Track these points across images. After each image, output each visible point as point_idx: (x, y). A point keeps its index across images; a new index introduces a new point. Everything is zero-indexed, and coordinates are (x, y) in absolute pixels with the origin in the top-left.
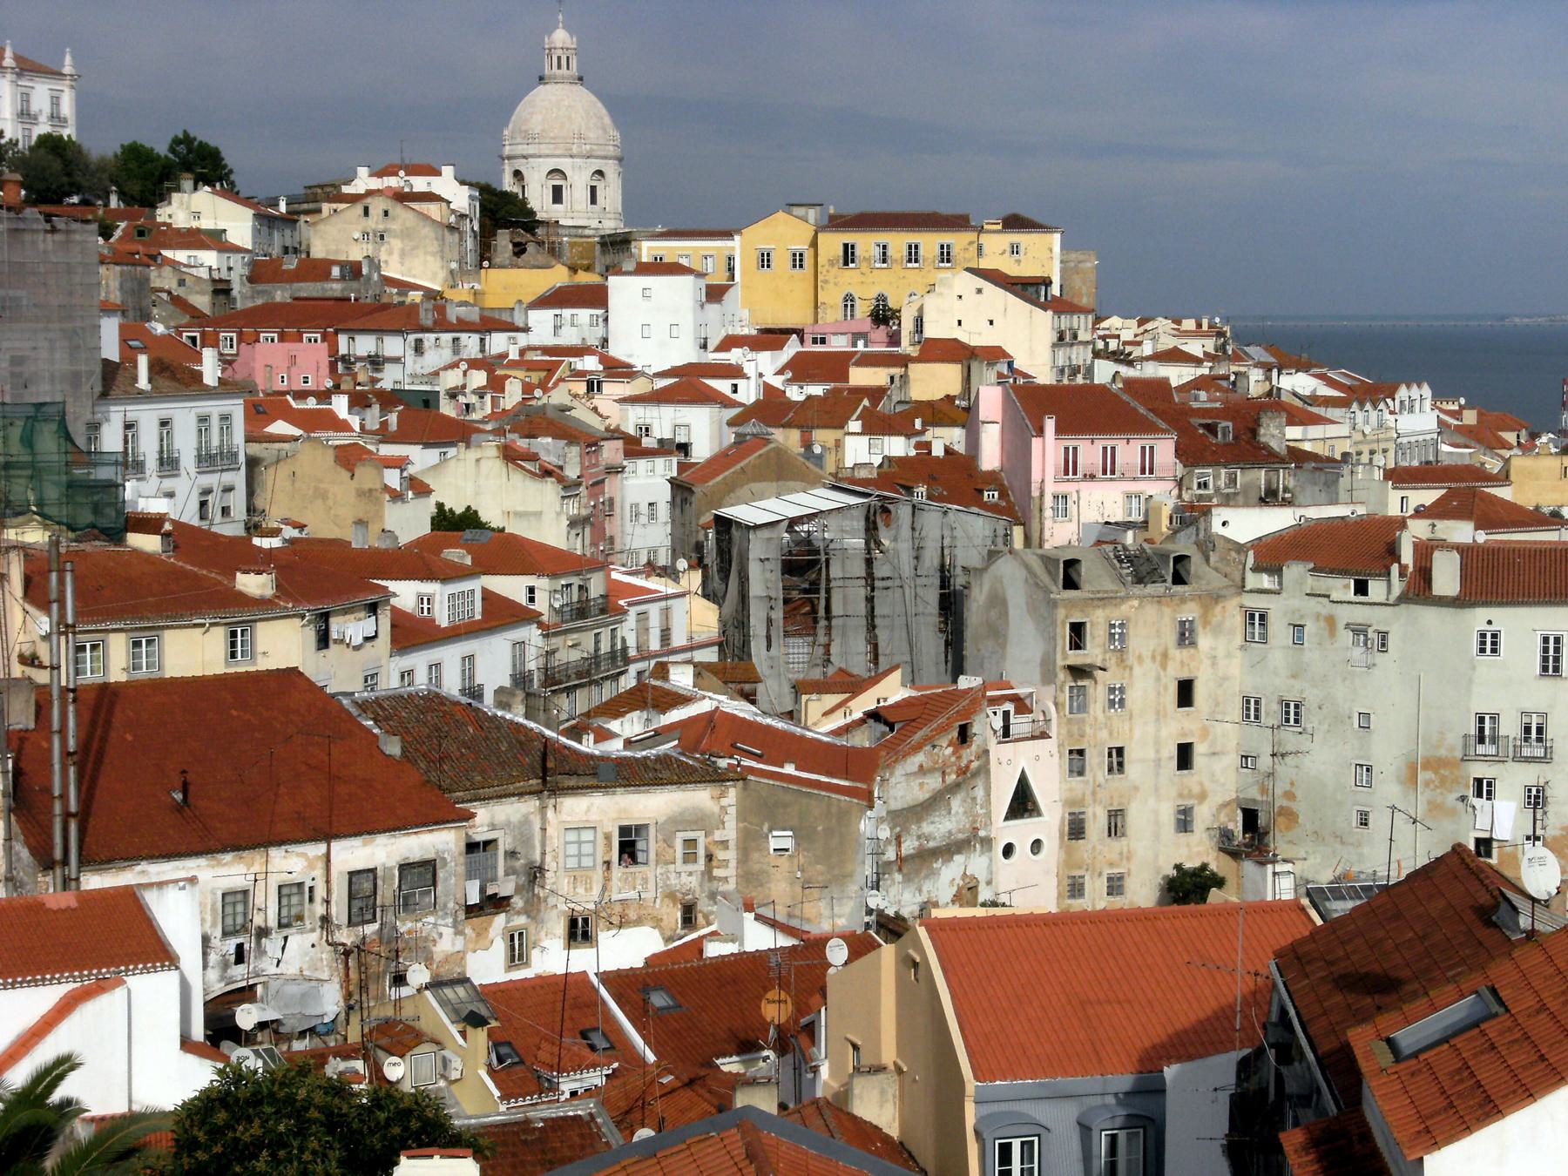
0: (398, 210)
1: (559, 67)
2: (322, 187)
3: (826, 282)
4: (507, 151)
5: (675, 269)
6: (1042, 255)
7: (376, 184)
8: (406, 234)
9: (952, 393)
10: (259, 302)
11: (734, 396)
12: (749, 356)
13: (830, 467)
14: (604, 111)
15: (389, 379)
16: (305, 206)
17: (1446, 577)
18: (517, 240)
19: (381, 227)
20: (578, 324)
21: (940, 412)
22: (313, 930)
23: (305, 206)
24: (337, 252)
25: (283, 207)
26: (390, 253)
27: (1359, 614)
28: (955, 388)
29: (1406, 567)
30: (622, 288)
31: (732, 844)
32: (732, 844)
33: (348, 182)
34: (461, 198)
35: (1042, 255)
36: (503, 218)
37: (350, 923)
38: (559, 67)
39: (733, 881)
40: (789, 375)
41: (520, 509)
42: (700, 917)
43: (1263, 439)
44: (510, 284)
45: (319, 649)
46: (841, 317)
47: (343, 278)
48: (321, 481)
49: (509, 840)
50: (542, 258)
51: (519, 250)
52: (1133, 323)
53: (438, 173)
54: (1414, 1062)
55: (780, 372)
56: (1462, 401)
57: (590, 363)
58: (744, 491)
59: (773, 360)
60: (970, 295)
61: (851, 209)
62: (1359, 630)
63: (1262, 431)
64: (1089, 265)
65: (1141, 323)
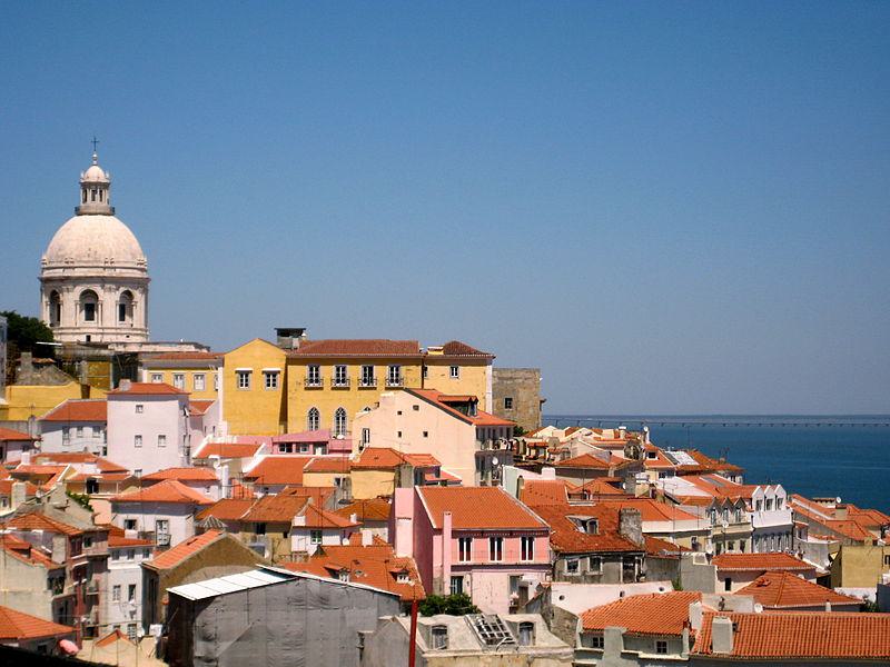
14: (133, 238)
30: (121, 413)
35: (476, 382)
46: (307, 428)
56: (839, 500)
63: (623, 525)
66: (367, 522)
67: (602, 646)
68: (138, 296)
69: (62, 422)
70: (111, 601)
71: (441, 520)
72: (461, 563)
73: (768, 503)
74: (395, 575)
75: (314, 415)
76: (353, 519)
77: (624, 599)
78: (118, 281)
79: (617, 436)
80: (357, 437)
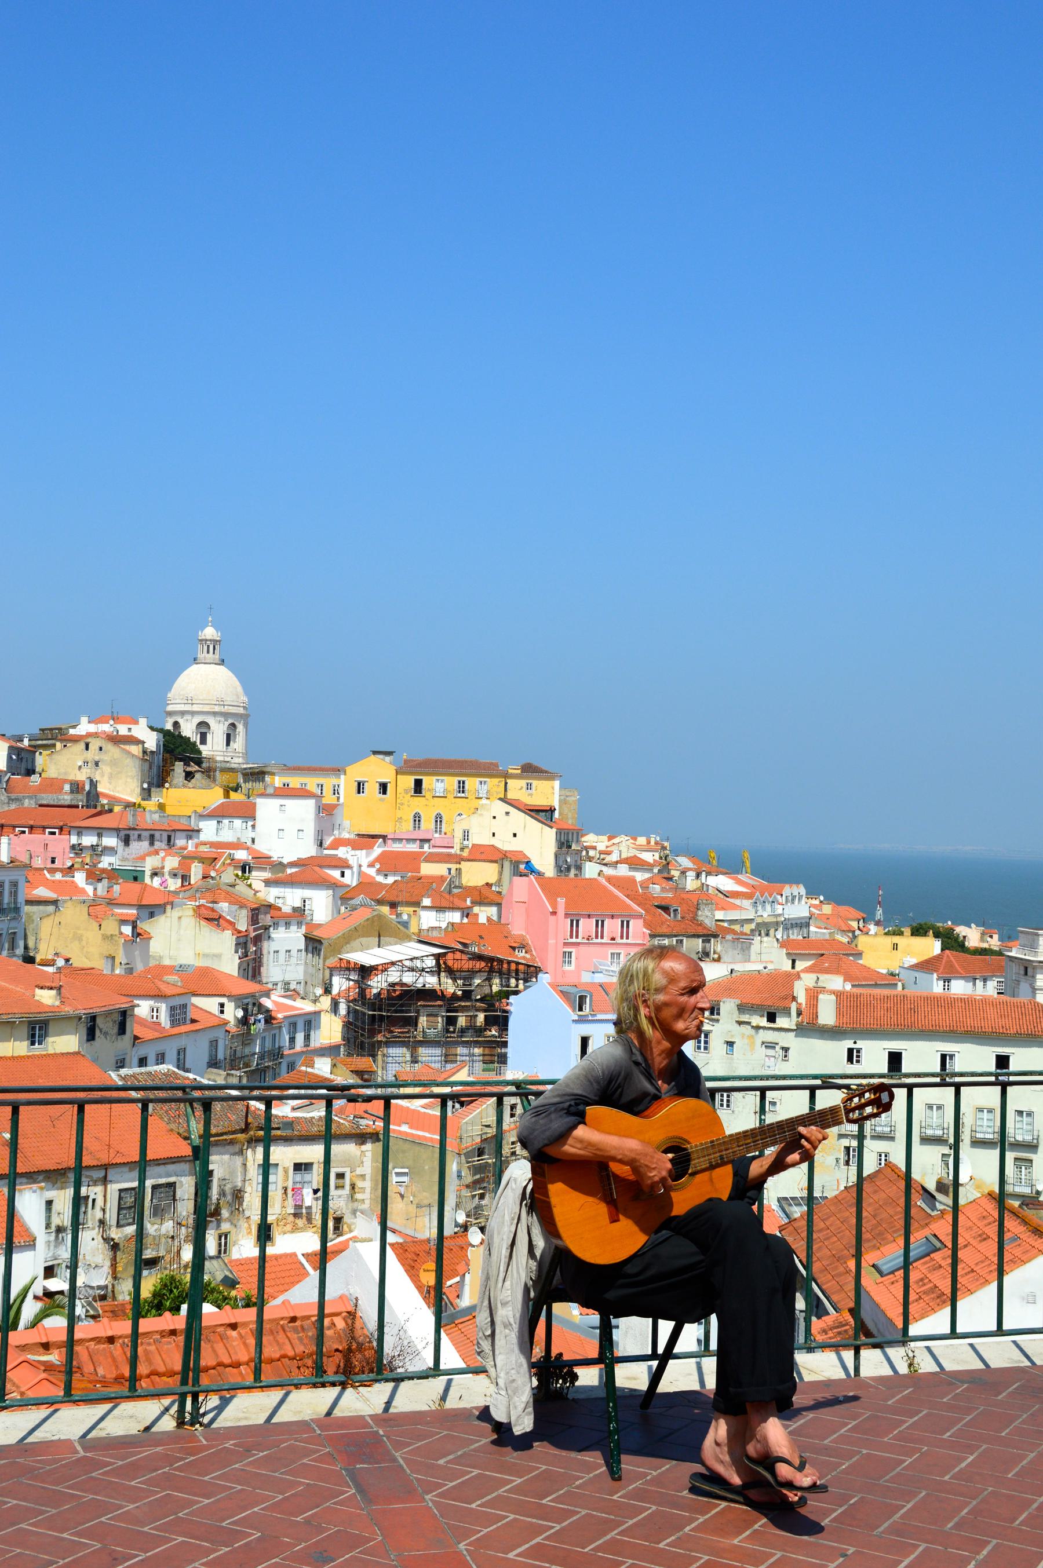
0: (109, 747)
1: (208, 652)
2: (51, 730)
3: (402, 804)
4: (170, 708)
5: (302, 793)
6: (547, 793)
7: (92, 728)
8: (114, 763)
9: (490, 882)
10: (13, 806)
11: (342, 879)
12: (353, 852)
13: (413, 928)
14: (238, 683)
15: (106, 862)
16: (40, 742)
17: (827, 1016)
18: (189, 769)
19: (97, 758)
20: (232, 830)
21: (484, 896)
22: (93, 1229)
23: (40, 742)
24: (66, 773)
25: (26, 742)
26: (103, 776)
27: (770, 1036)
28: (493, 879)
29: (800, 1004)
30: (266, 807)
31: (368, 1177)
32: (368, 1177)
33: (74, 727)
34: (151, 740)
35: (547, 793)
36: (176, 754)
37: (119, 1225)
38: (208, 652)
39: (367, 1202)
40: (378, 866)
41: (207, 951)
42: (345, 1227)
43: (700, 918)
44: (183, 797)
45: (88, 1040)
46: (411, 828)
47: (72, 792)
48: (78, 928)
49: (221, 1171)
50: (205, 781)
51: (189, 776)
52: (605, 838)
53: (136, 723)
54: (892, 1276)
55: (371, 865)
56: (822, 898)
57: (241, 855)
58: (356, 943)
59: (367, 855)
60: (500, 815)
61: (420, 757)
62: (770, 1046)
63: (700, 913)
64: (573, 799)
65: (610, 838)
66: (482, 901)
67: (718, 1014)
68: (240, 728)
69: (218, 814)
70: (271, 964)
71: (554, 904)
72: (571, 940)
73: (794, 898)
74: (514, 948)
75: (417, 819)
76: (468, 902)
77: (734, 975)
78: (226, 715)
79: (649, 842)
80: (459, 835)
